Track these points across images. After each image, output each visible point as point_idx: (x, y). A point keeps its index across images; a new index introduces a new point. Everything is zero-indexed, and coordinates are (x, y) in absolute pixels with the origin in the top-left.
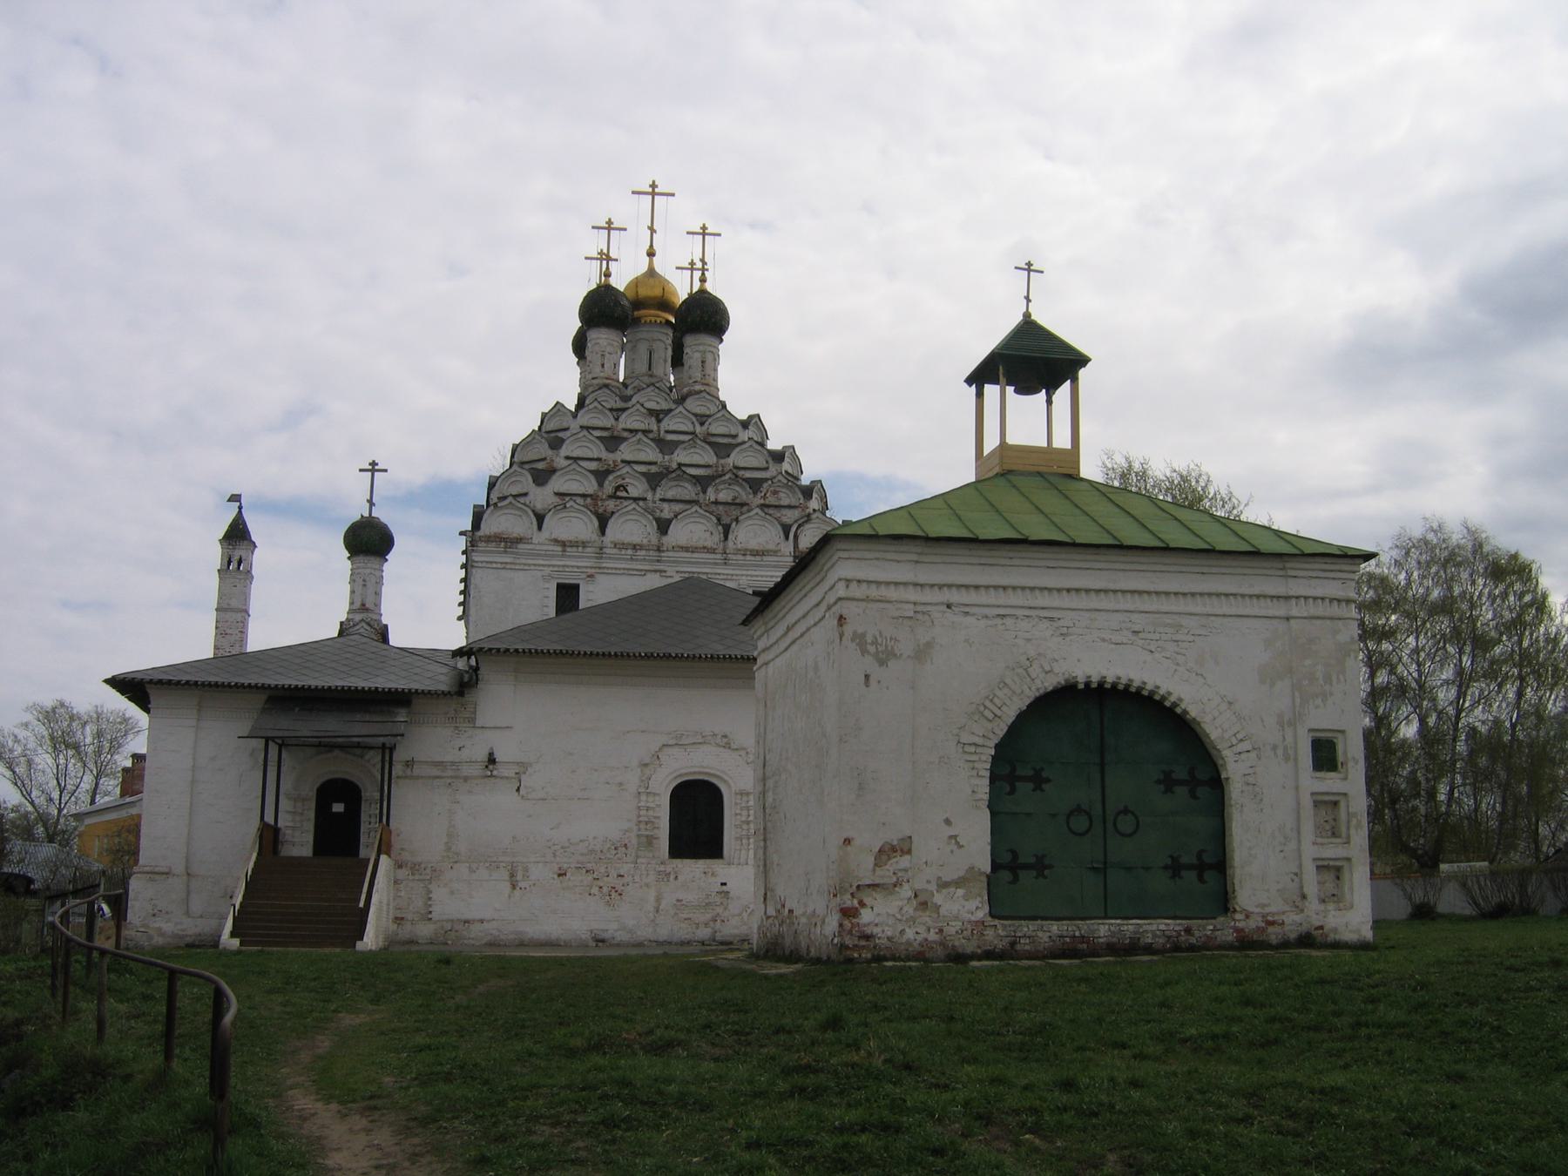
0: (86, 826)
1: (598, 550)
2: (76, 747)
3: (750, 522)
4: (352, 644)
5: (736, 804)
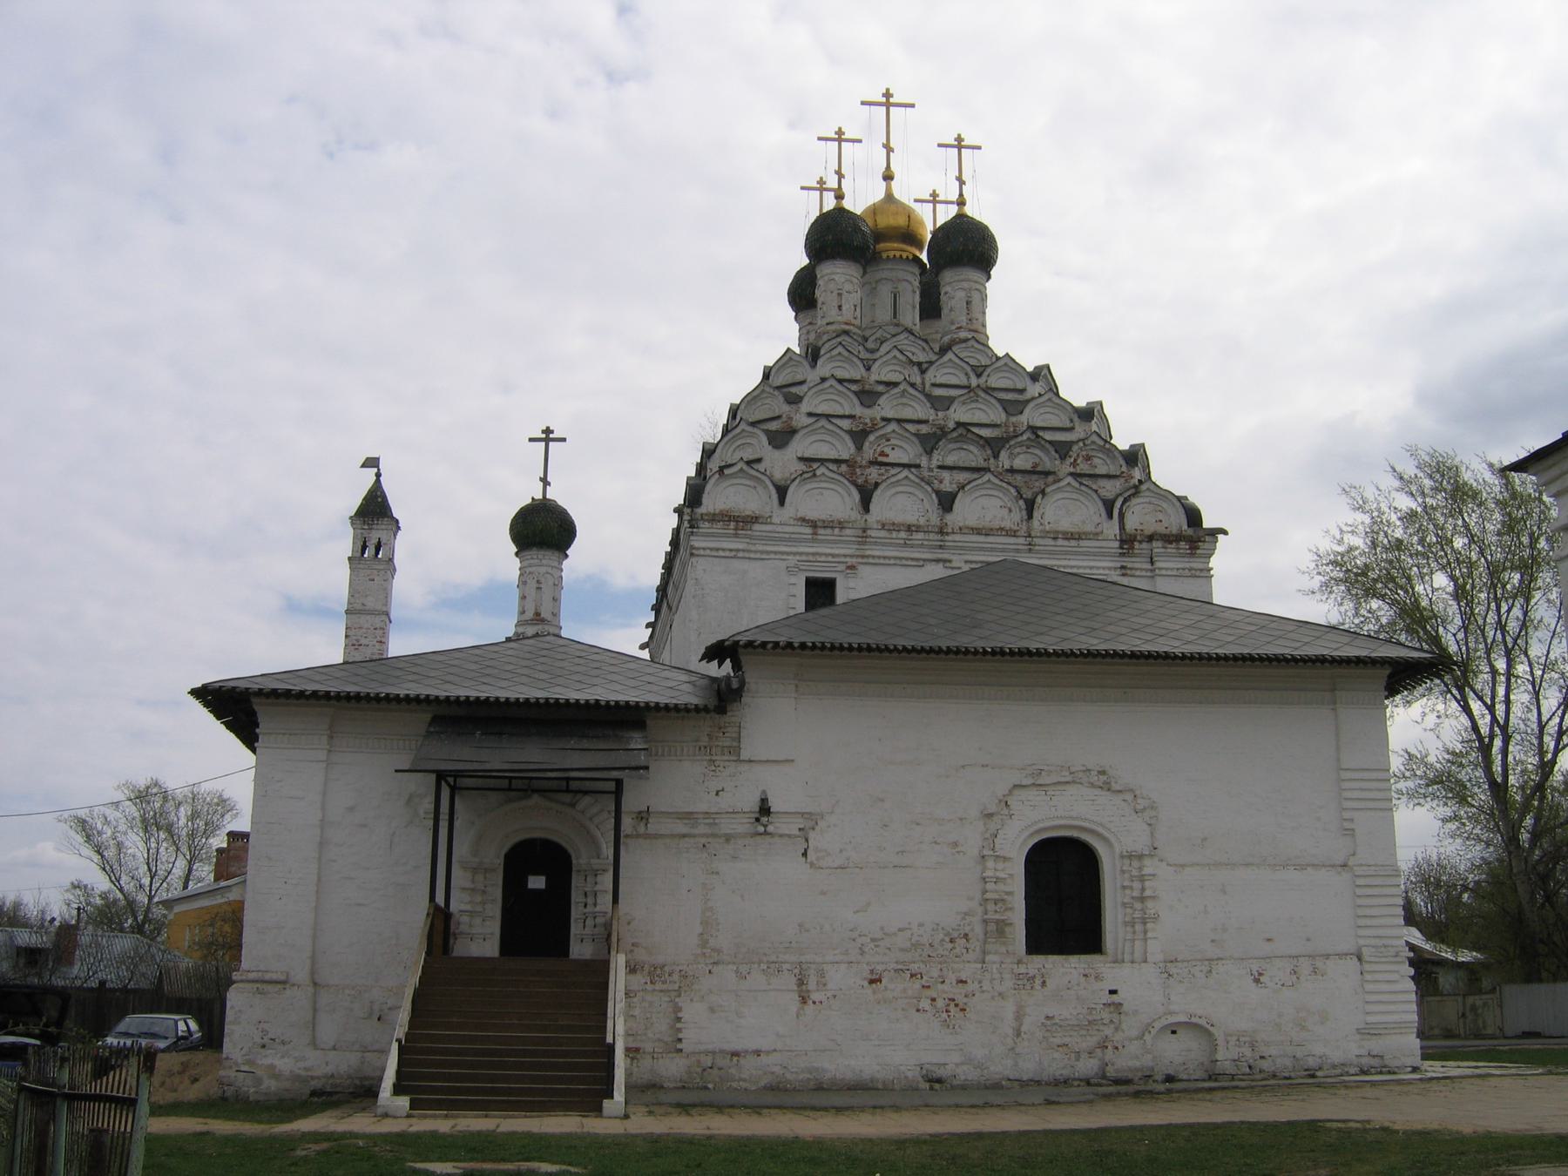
0: (176, 914)
1: (860, 533)
2: (169, 829)
3: (1060, 495)
4: (547, 646)
5: (1123, 872)
